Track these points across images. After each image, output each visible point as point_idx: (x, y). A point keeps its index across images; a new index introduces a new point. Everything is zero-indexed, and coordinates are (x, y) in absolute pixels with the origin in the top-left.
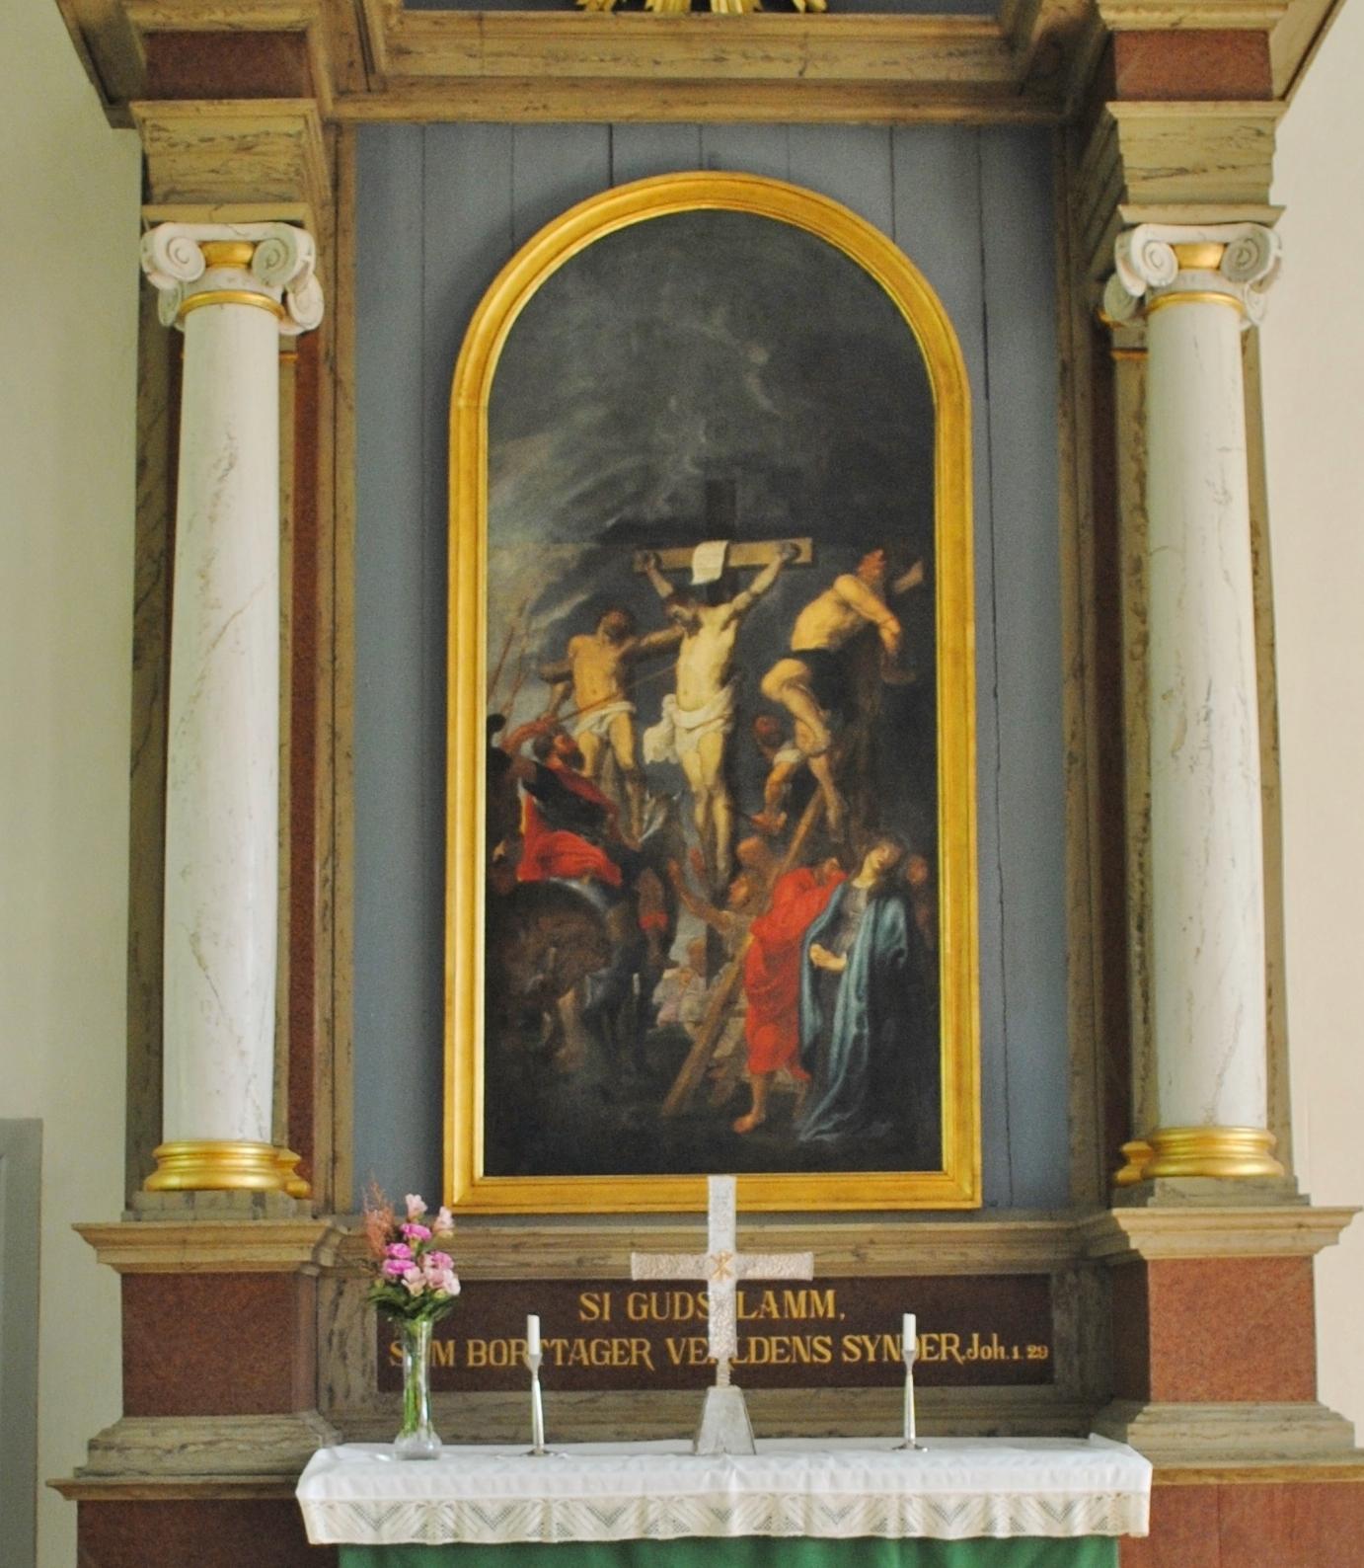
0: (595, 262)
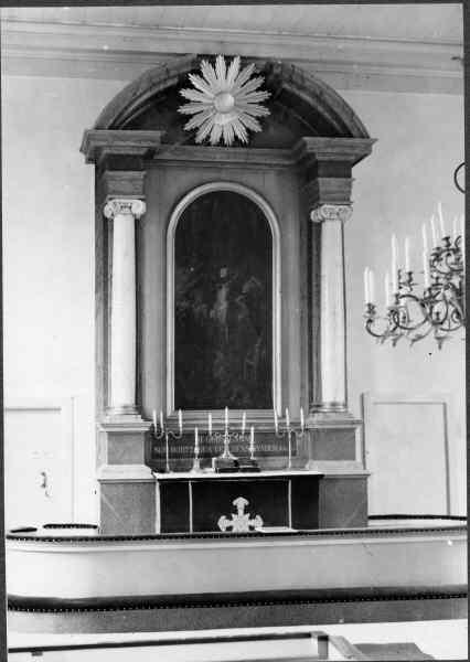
0: (199, 200)
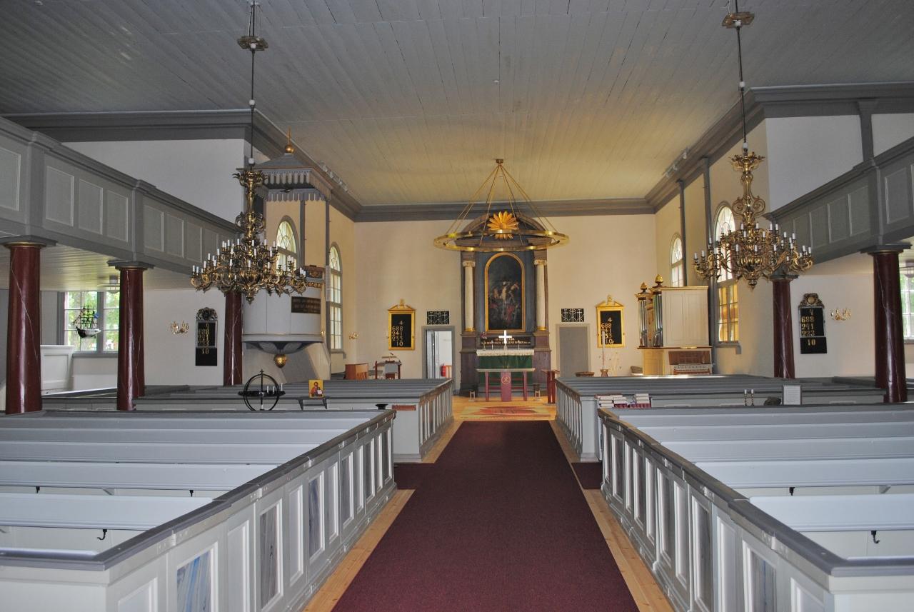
0: (495, 259)
